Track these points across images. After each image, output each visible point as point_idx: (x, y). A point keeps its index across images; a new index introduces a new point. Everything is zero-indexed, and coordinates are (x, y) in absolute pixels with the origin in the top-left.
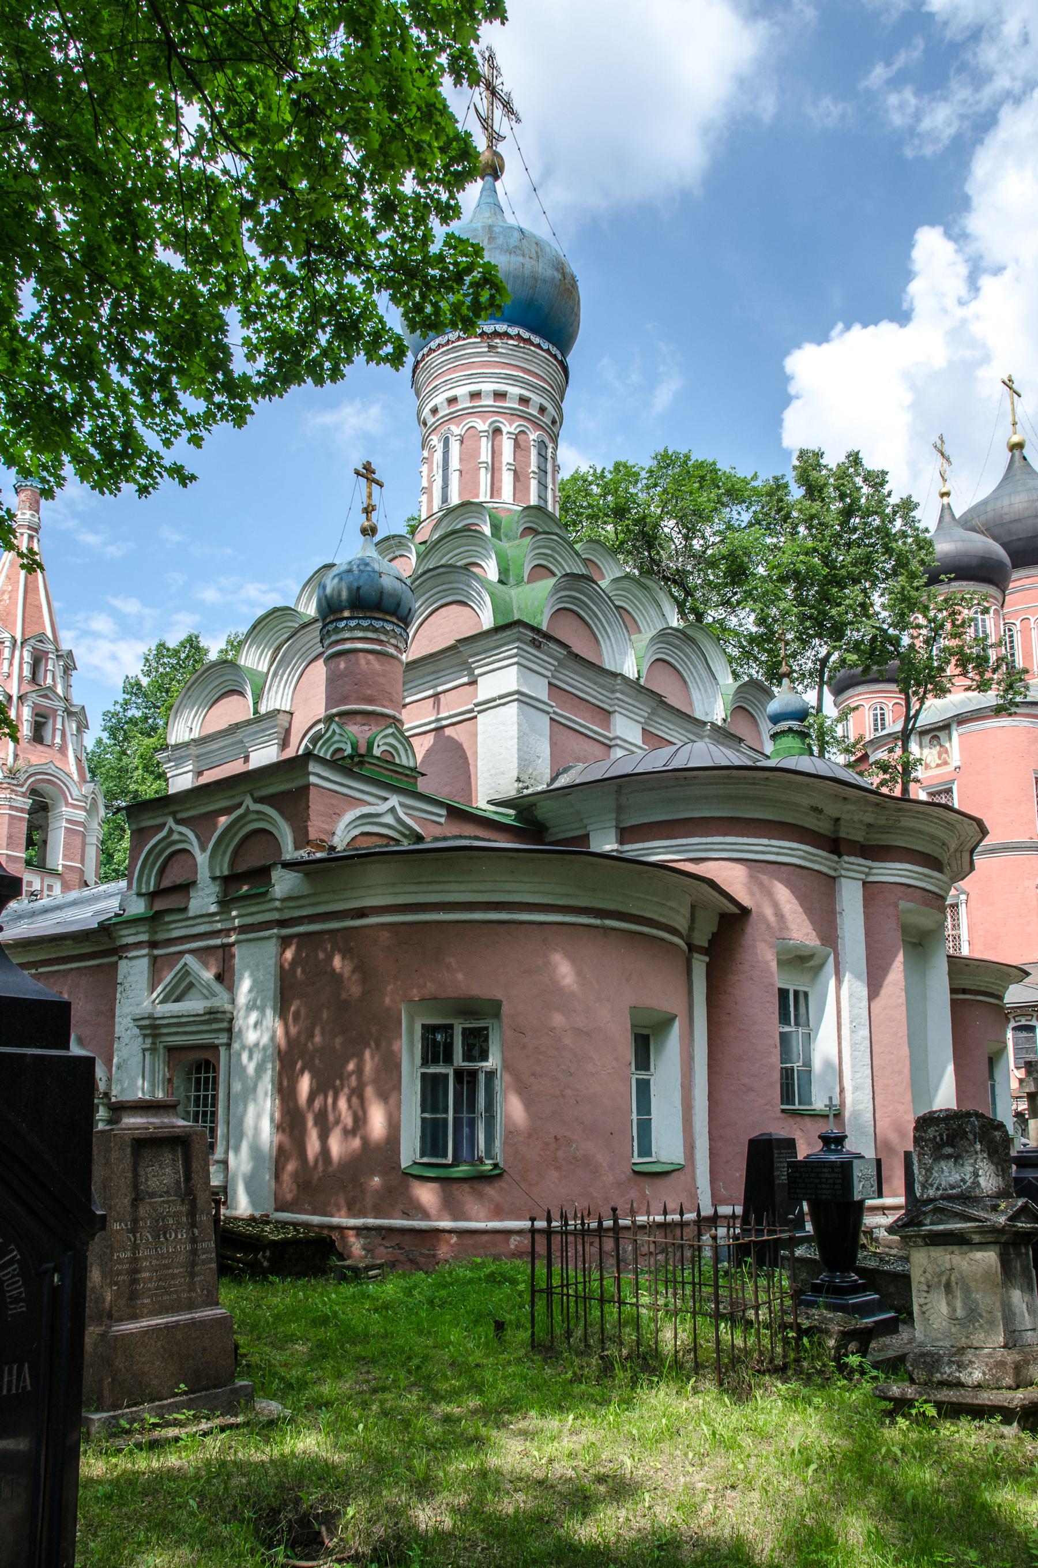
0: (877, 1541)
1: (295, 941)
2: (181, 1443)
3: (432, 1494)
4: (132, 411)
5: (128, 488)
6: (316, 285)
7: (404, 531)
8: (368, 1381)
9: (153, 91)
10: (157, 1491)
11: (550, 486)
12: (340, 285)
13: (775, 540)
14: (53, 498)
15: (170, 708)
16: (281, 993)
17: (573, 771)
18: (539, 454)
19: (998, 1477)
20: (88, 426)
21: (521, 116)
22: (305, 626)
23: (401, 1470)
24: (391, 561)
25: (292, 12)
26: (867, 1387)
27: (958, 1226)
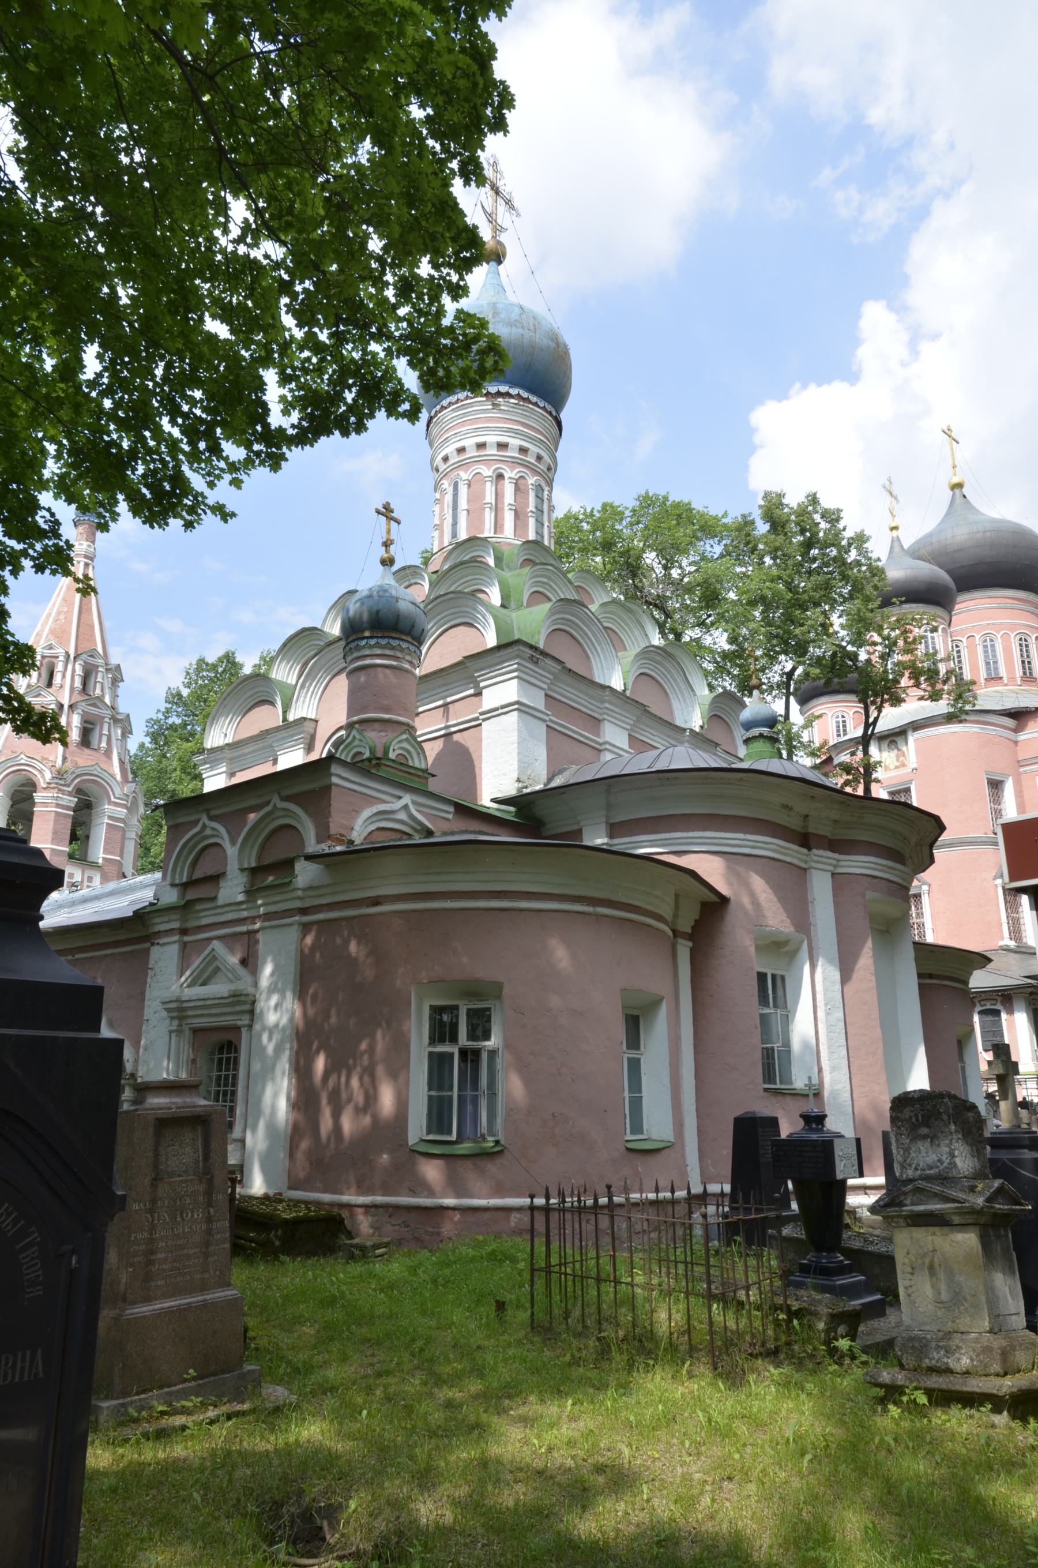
0: (874, 1537)
1: (315, 927)
2: (188, 1432)
3: (434, 1485)
4: (181, 457)
5: (175, 524)
6: (344, 351)
7: (417, 561)
8: (372, 1365)
9: (206, 189)
10: (161, 1483)
11: (546, 524)
12: (365, 352)
13: (744, 569)
14: (108, 531)
15: (207, 716)
16: (301, 976)
17: (567, 773)
18: (537, 496)
19: (991, 1469)
20: (141, 469)
21: (520, 212)
22: (330, 644)
23: (404, 1460)
24: (406, 587)
25: (325, 125)
26: (858, 1372)
27: (938, 1206)
